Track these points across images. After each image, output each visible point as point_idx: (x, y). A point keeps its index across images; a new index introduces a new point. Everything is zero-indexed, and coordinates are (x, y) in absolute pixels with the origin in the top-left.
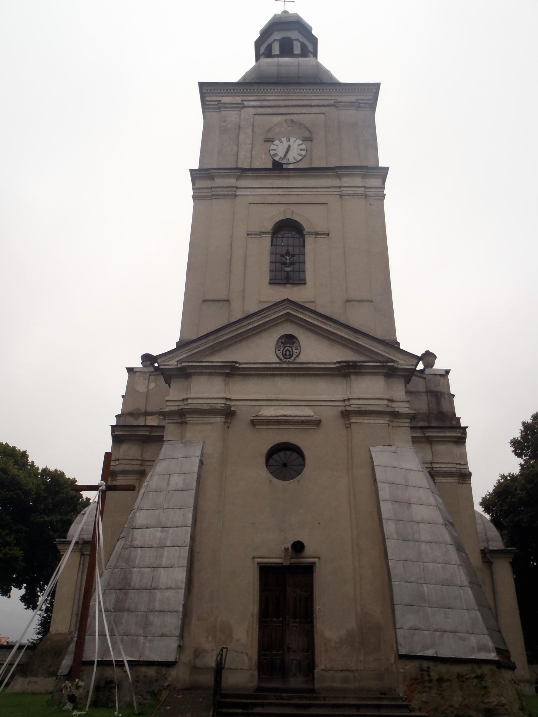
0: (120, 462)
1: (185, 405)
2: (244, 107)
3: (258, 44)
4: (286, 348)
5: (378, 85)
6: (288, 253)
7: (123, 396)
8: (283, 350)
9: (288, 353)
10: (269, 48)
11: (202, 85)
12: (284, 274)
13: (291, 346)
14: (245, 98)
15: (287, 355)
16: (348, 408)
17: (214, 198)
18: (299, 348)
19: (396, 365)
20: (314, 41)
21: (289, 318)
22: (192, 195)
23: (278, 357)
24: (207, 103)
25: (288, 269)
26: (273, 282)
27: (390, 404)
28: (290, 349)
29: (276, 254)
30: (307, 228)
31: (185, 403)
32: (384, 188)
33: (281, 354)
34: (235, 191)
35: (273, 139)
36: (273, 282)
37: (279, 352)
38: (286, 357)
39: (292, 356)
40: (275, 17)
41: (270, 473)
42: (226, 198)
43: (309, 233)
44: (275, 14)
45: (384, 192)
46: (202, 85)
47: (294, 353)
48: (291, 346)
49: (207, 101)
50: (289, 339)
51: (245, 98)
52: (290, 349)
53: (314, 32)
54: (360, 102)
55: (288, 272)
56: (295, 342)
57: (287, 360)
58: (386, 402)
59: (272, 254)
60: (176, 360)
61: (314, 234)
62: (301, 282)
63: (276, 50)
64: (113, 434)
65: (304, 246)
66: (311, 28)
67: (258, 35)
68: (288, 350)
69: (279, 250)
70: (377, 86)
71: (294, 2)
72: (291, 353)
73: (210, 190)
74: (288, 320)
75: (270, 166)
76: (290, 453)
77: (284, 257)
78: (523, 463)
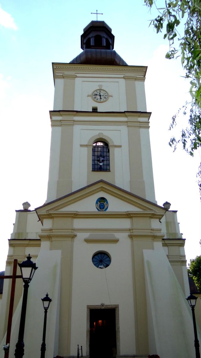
1: (51, 232)
2: (77, 77)
3: (83, 37)
5: (147, 67)
6: (101, 156)
7: (14, 224)
8: (100, 205)
10: (89, 41)
11: (53, 63)
12: (99, 166)
14: (76, 72)
16: (132, 234)
19: (155, 213)
20: (113, 37)
21: (103, 189)
23: (97, 209)
24: (57, 74)
25: (101, 164)
26: (94, 170)
27: (152, 231)
28: (103, 204)
29: (95, 156)
31: (51, 231)
32: (149, 123)
34: (73, 123)
35: (161, 229)
40: (93, 22)
43: (111, 146)
45: (149, 125)
46: (53, 63)
47: (105, 206)
49: (57, 73)
50: (102, 200)
51: (76, 72)
52: (103, 204)
53: (113, 33)
55: (101, 166)
57: (102, 210)
58: (150, 231)
59: (93, 156)
62: (108, 170)
63: (92, 43)
64: (10, 243)
65: (109, 152)
66: (111, 30)
67: (82, 33)
68: (102, 205)
69: (96, 154)
70: (146, 68)
71: (102, 14)
72: (104, 206)
73: (60, 122)
74: (102, 190)
75: (91, 110)
76: (103, 255)
77: (99, 158)
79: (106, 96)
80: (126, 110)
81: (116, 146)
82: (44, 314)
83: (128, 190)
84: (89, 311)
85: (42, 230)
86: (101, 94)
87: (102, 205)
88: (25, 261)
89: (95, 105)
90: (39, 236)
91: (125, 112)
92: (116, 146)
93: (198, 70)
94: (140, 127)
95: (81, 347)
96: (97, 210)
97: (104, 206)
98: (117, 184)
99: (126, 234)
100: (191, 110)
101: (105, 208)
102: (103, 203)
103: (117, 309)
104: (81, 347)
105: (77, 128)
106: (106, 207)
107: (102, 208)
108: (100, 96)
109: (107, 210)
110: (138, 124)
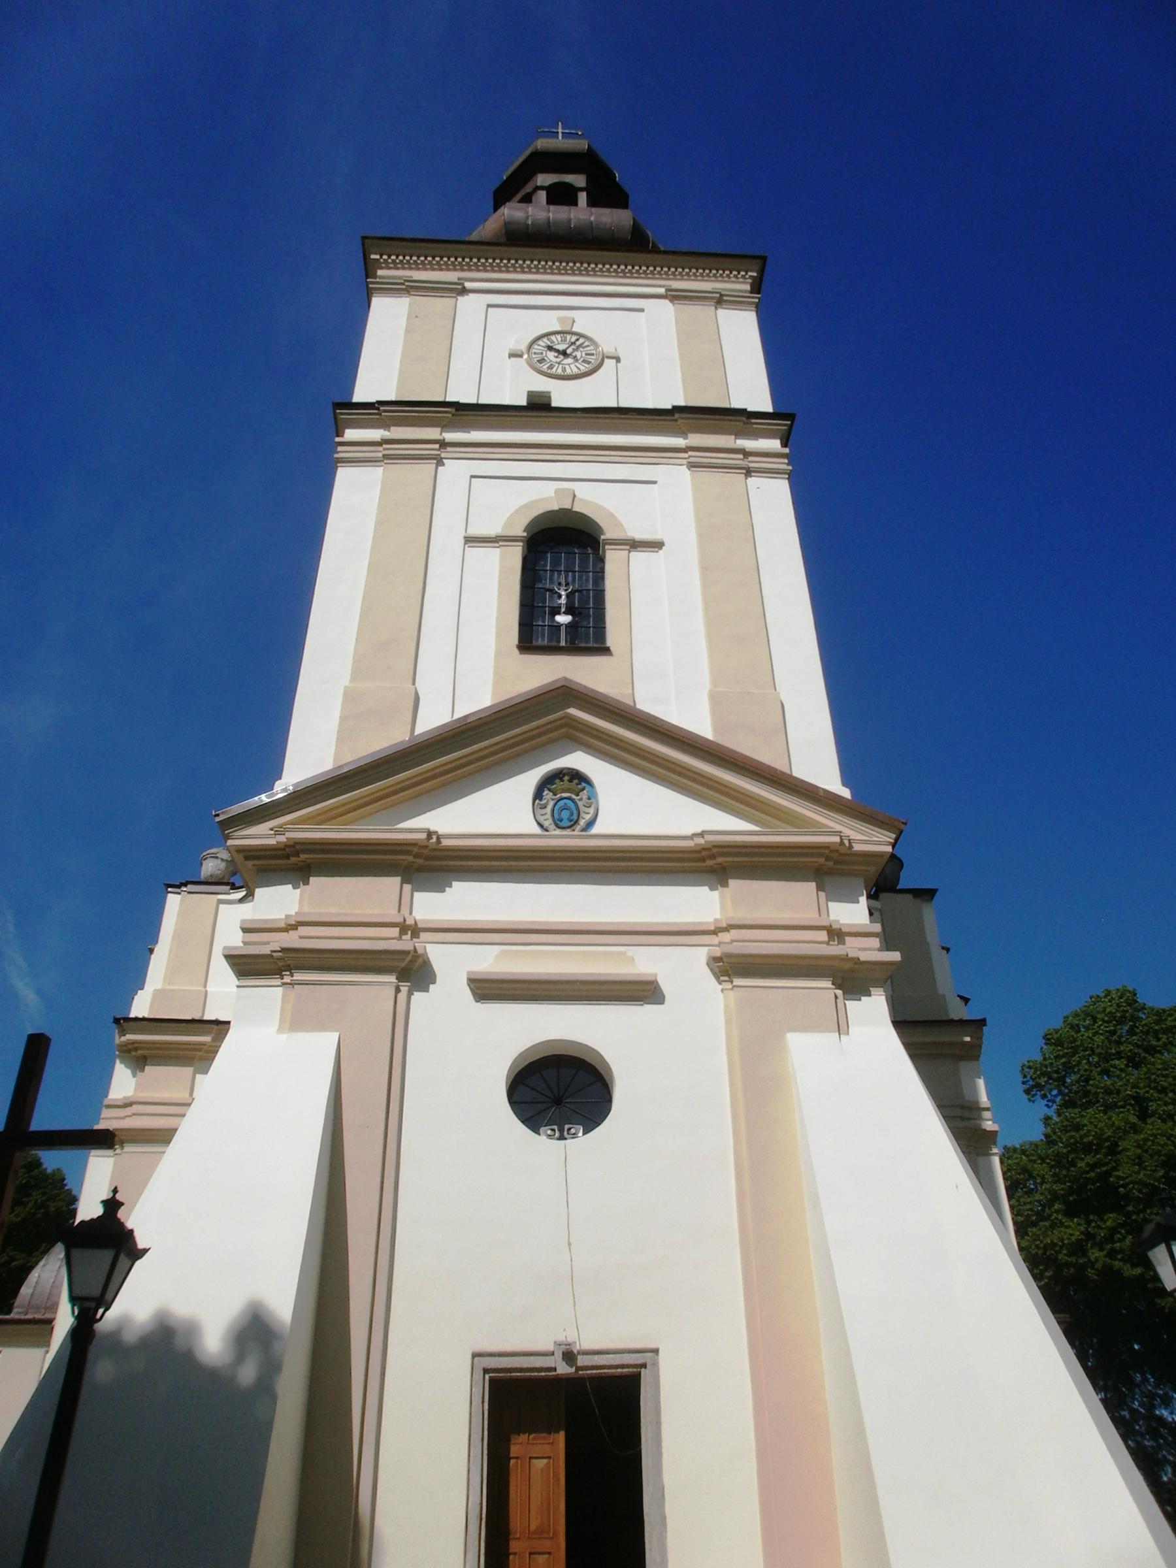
0: (136, 1108)
2: (464, 291)
4: (561, 803)
9: (565, 815)
13: (574, 796)
15: (568, 819)
17: (386, 463)
18: (595, 802)
22: (434, 983)
23: (541, 825)
28: (569, 803)
30: (609, 533)
33: (549, 816)
36: (528, 642)
37: (546, 817)
38: (561, 824)
39: (576, 822)
41: (898, 1024)
42: (483, 1402)
44: (477, 1001)
47: (582, 814)
48: (574, 796)
54: (723, 293)
56: (583, 789)
60: (271, 827)
61: (627, 545)
72: (575, 817)
75: (523, 402)
78: (1051, 1112)
79: (593, 354)
80: (681, 402)
81: (634, 545)
82: (423, 622)
83: (700, 723)
84: (482, 1392)
85: (245, 930)
86: (569, 360)
87: (565, 808)
88: (92, 1220)
89: (541, 384)
90: (228, 957)
91: (676, 409)
92: (634, 545)
93: (1113, 1139)
94: (749, 472)
95: (642, 310)
96: (537, 830)
97: (575, 812)
98: (648, 703)
99: (697, 957)
100: (1046, 1035)
101: (582, 822)
102: (569, 798)
103: (646, 1376)
104: (642, 310)
105: (455, 471)
106: (588, 817)
107: (565, 823)
108: (564, 353)
109: (595, 830)
110: (737, 460)
